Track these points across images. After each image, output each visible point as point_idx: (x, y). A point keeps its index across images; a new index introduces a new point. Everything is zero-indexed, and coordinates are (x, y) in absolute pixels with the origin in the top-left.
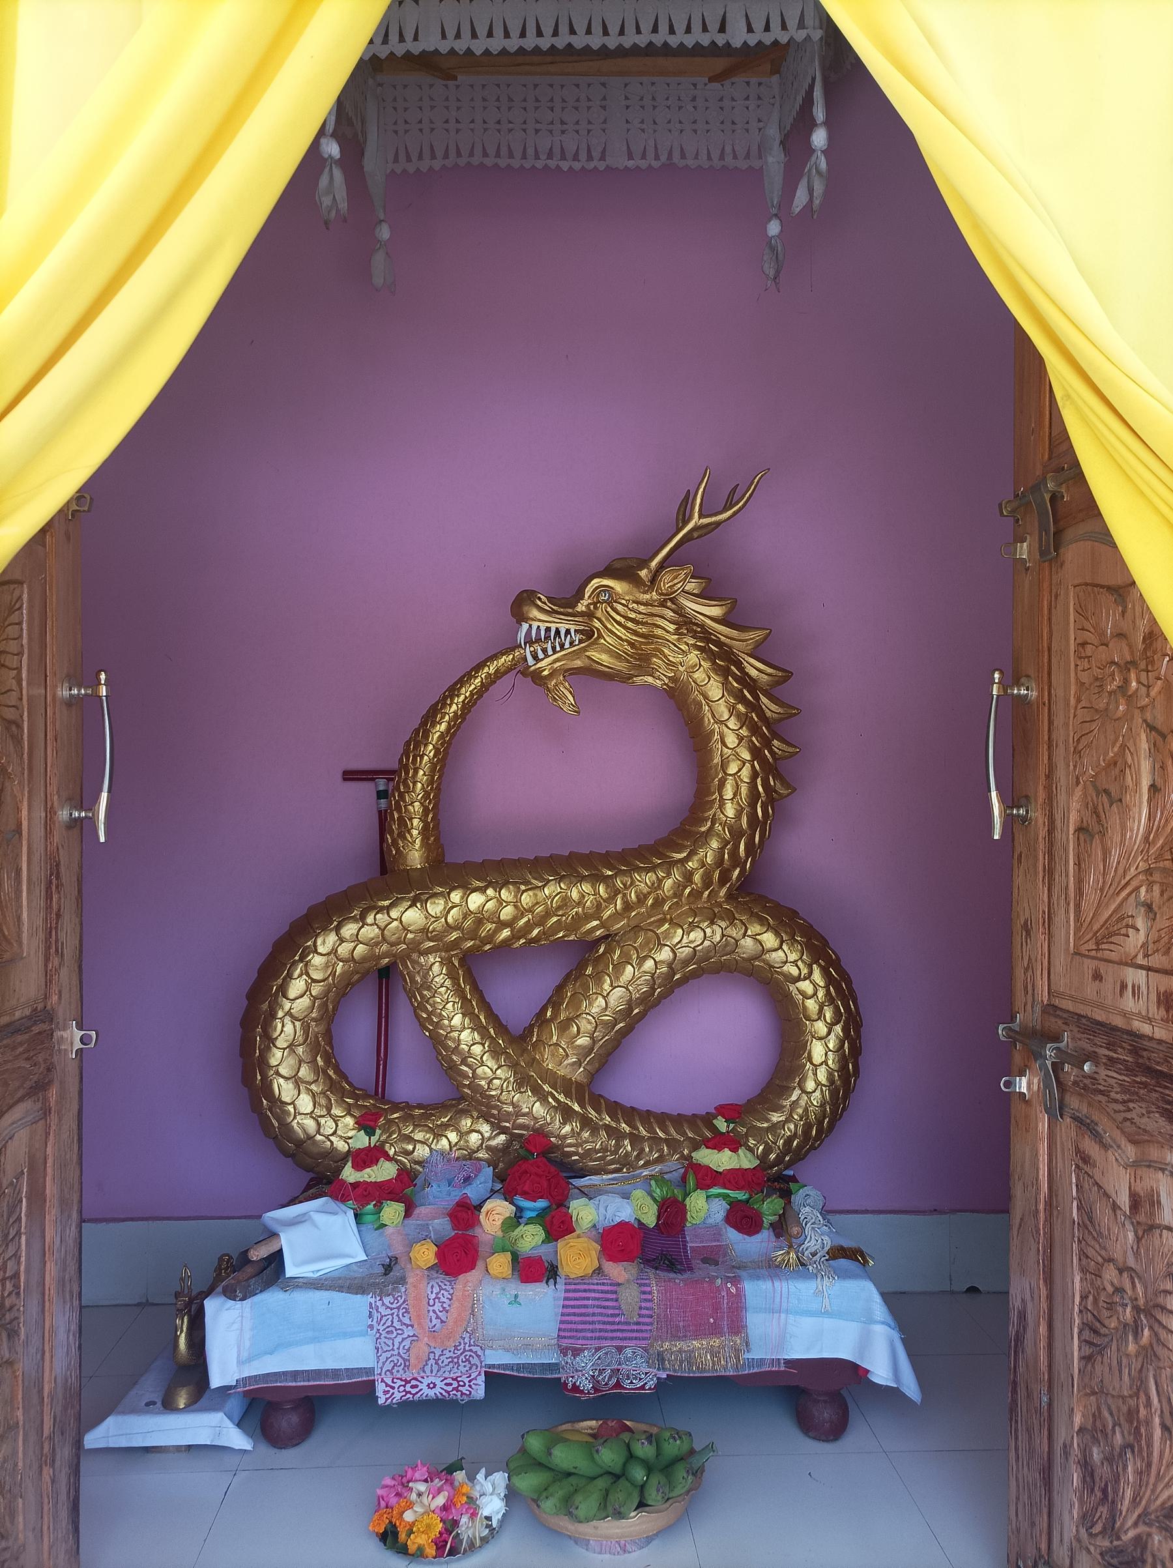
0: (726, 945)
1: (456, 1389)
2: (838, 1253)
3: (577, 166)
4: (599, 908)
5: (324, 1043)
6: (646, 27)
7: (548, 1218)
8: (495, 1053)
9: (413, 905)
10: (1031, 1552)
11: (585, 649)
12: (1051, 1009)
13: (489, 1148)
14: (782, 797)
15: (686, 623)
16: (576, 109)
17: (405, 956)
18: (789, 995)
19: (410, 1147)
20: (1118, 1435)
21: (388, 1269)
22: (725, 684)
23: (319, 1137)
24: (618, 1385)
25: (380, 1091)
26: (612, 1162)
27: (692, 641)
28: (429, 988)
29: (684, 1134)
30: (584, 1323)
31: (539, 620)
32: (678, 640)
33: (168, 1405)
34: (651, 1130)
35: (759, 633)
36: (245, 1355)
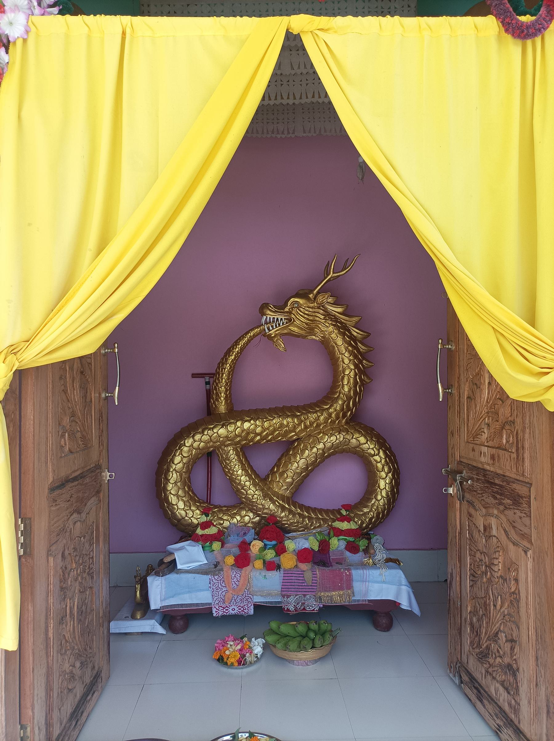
0: (345, 441)
1: (243, 611)
2: (388, 560)
3: (283, 136)
4: (295, 427)
5: (187, 482)
6: (310, 96)
7: (277, 547)
8: (255, 485)
9: (222, 427)
10: (455, 660)
11: (288, 326)
12: (460, 462)
13: (252, 522)
14: (367, 383)
15: (328, 315)
16: (283, 114)
17: (219, 447)
18: (370, 462)
19: (222, 522)
20: (481, 611)
21: (216, 566)
22: (344, 339)
23: (186, 518)
24: (304, 609)
25: (208, 500)
26: (301, 527)
27: (330, 322)
28: (229, 460)
29: (329, 516)
30: (291, 585)
31: (270, 315)
32: (325, 322)
33: (133, 617)
34: (316, 515)
35: (357, 318)
36: (163, 597)
